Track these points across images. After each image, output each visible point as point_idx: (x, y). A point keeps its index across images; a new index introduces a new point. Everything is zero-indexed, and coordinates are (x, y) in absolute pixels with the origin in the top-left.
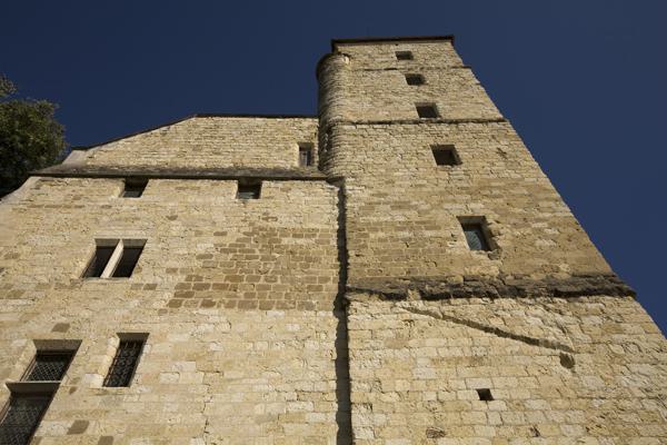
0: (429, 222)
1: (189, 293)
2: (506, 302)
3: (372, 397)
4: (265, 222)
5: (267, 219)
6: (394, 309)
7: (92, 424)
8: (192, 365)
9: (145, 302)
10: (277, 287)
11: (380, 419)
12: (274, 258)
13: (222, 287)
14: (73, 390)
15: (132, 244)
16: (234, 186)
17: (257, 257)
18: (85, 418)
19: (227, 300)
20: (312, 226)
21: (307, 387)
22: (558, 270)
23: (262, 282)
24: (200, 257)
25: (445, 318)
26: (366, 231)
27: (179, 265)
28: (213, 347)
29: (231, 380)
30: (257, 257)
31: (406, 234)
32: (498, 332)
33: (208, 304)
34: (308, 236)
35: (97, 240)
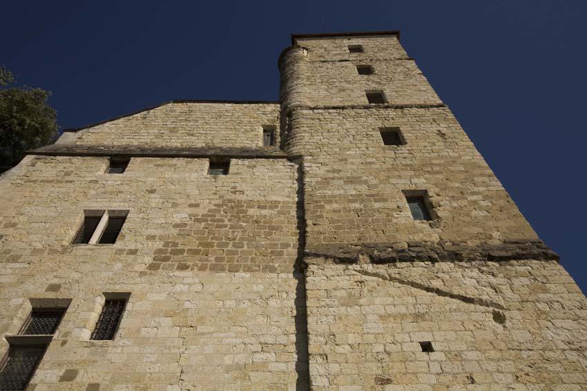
0: (376, 195)
2: (445, 266)
3: (327, 349)
4: (233, 196)
5: (234, 193)
6: (347, 272)
7: (81, 373)
8: (169, 321)
10: (243, 252)
11: (334, 368)
12: (241, 227)
13: (196, 252)
14: (64, 343)
15: (116, 215)
16: (206, 163)
17: (226, 226)
18: (75, 367)
19: (200, 264)
20: (274, 198)
21: (270, 340)
22: (491, 237)
23: (230, 247)
24: (176, 226)
25: (391, 279)
26: (322, 203)
27: (158, 232)
28: (187, 305)
29: (203, 334)
30: (226, 226)
31: (357, 205)
32: (439, 292)
33: (183, 267)
34: (271, 208)
35: (85, 211)
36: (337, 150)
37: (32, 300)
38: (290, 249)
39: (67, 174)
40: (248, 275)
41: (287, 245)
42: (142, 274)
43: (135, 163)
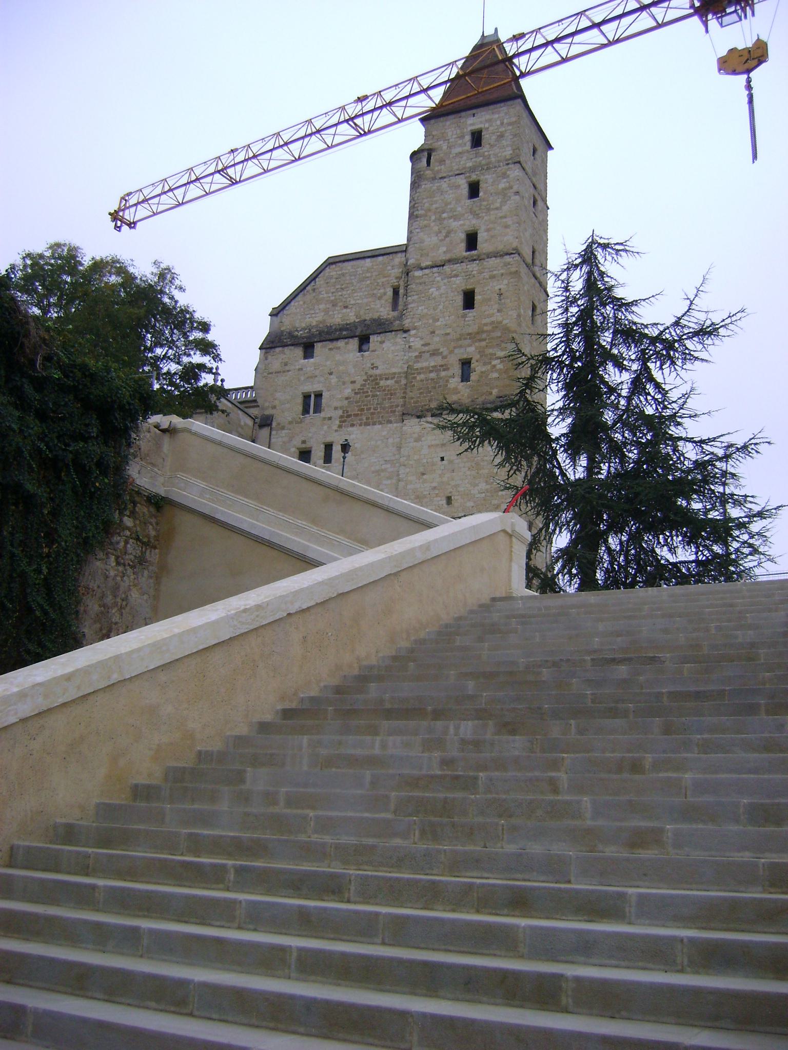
5: (372, 368)
9: (329, 427)
11: (408, 470)
12: (377, 396)
17: (369, 396)
20: (394, 370)
21: (387, 459)
24: (347, 399)
30: (369, 396)
31: (433, 375)
33: (353, 425)
34: (392, 378)
36: (431, 321)
37: (298, 448)
38: (399, 408)
39: (286, 365)
42: (336, 431)
43: (318, 347)
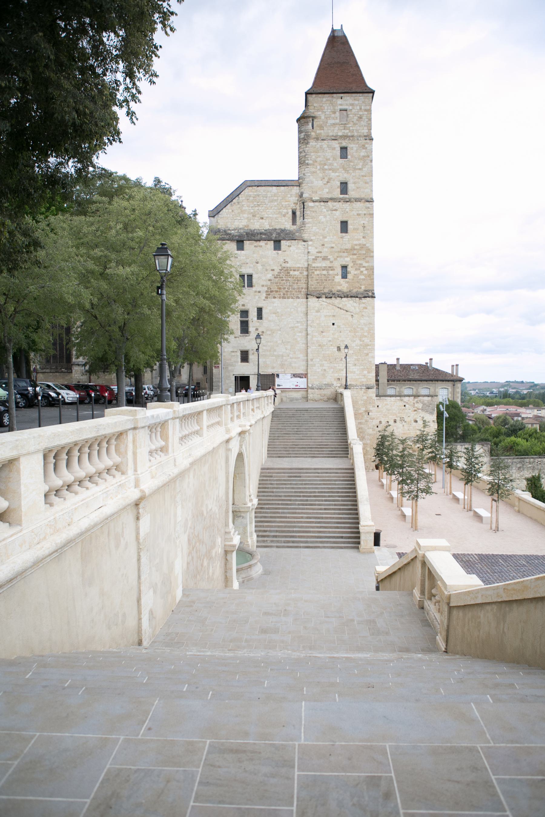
1: (269, 293)
5: (285, 262)
11: (313, 329)
13: (277, 291)
27: (265, 283)
28: (278, 310)
33: (275, 298)
40: (292, 300)
41: (302, 288)
